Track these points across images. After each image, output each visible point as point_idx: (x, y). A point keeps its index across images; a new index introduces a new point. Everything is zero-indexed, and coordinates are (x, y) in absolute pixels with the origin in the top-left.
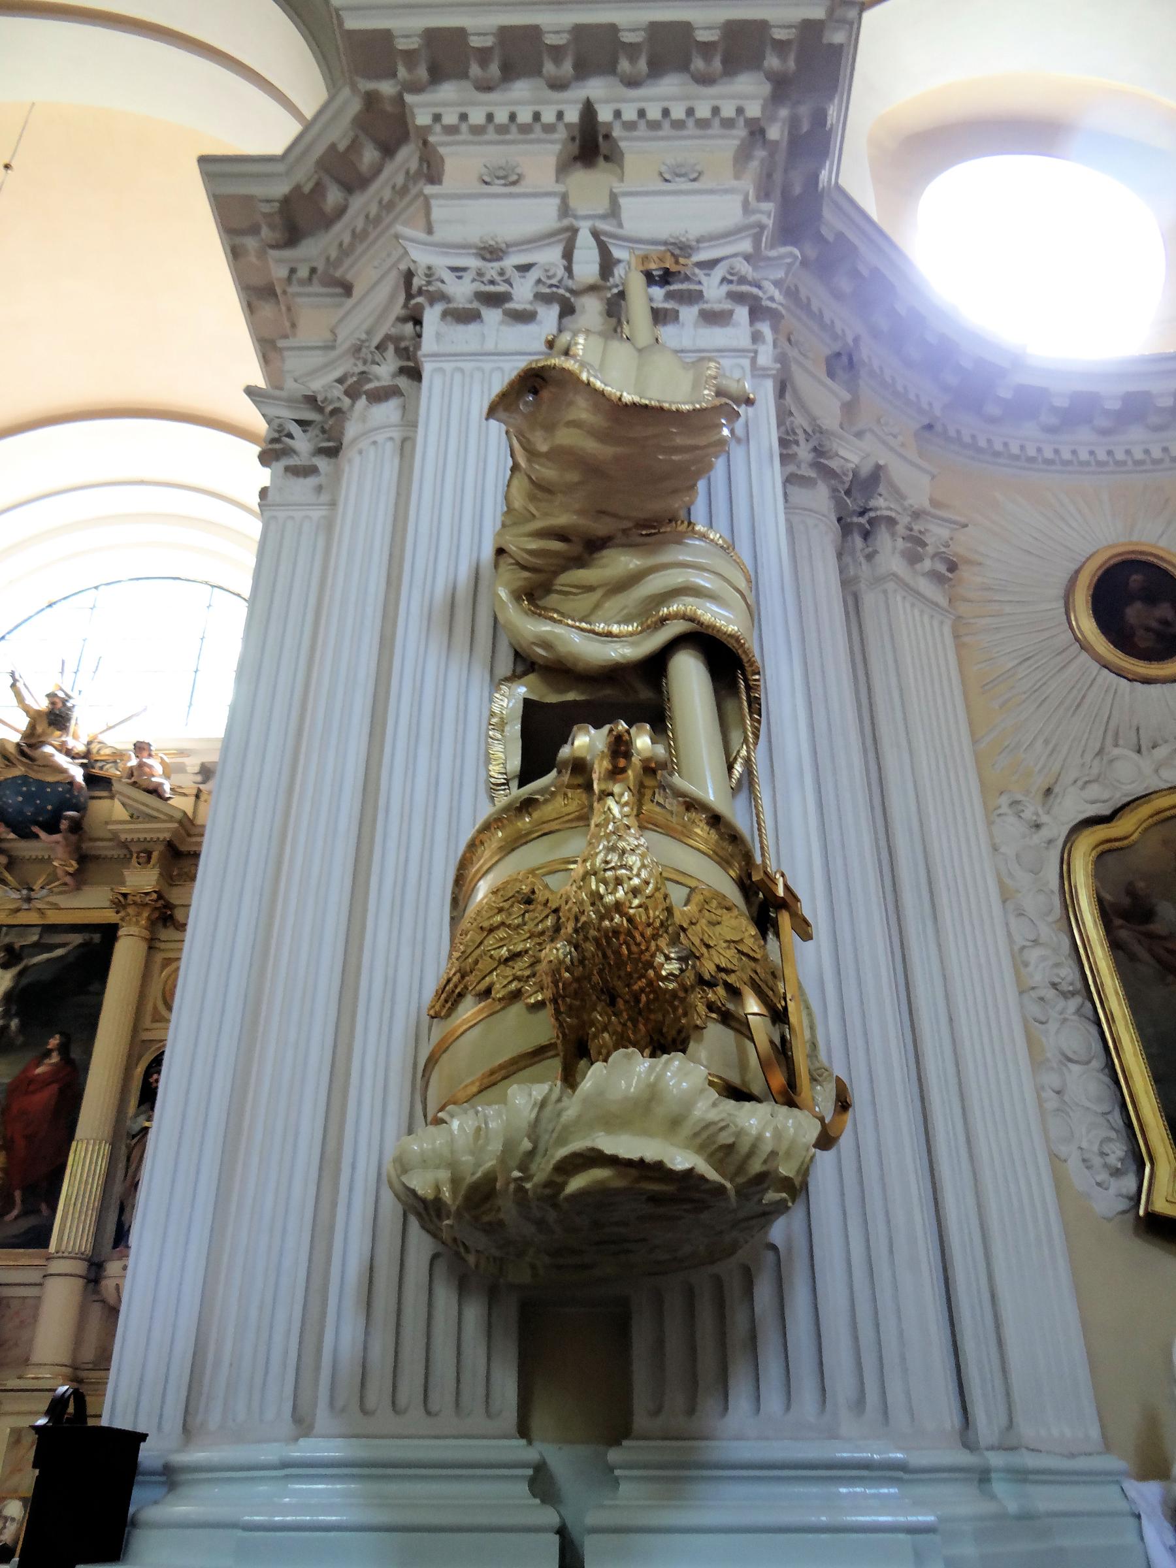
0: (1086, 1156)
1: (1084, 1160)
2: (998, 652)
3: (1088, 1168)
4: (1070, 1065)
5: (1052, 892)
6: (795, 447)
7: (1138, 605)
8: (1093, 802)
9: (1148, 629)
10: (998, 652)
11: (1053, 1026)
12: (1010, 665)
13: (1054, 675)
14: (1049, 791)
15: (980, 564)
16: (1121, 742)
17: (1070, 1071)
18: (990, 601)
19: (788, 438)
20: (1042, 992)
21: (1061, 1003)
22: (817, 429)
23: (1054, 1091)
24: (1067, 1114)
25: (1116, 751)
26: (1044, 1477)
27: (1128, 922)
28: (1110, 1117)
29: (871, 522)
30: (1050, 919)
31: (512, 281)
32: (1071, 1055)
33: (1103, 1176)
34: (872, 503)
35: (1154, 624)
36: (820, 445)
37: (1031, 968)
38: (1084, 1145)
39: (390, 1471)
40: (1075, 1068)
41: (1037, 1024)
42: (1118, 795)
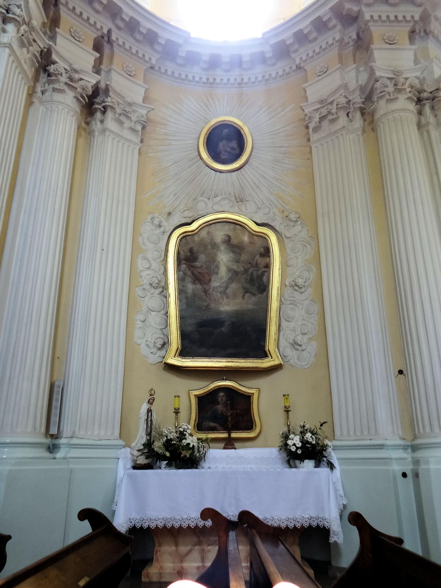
0: (148, 343)
1: (147, 345)
2: (164, 160)
3: (148, 347)
4: (151, 312)
5: (162, 251)
6: (60, 77)
7: (224, 142)
8: (185, 218)
9: (226, 151)
10: (164, 160)
11: (147, 299)
12: (168, 165)
13: (187, 168)
14: (169, 214)
15: (166, 125)
16: (204, 195)
17: (151, 314)
18: (166, 140)
19: (55, 72)
20: (145, 287)
21: (153, 290)
22: (72, 69)
23: (141, 321)
24: (145, 329)
25: (201, 198)
26: (351, 448)
27: (187, 262)
28: (164, 330)
29: (104, 107)
30: (159, 260)
31: (9, 4)
32: (152, 309)
33: (154, 350)
34: (106, 100)
35: (229, 149)
36: (70, 76)
37: (143, 278)
38: (149, 340)
39: (16, 445)
40: (154, 314)
41: (139, 298)
42: (196, 215)
